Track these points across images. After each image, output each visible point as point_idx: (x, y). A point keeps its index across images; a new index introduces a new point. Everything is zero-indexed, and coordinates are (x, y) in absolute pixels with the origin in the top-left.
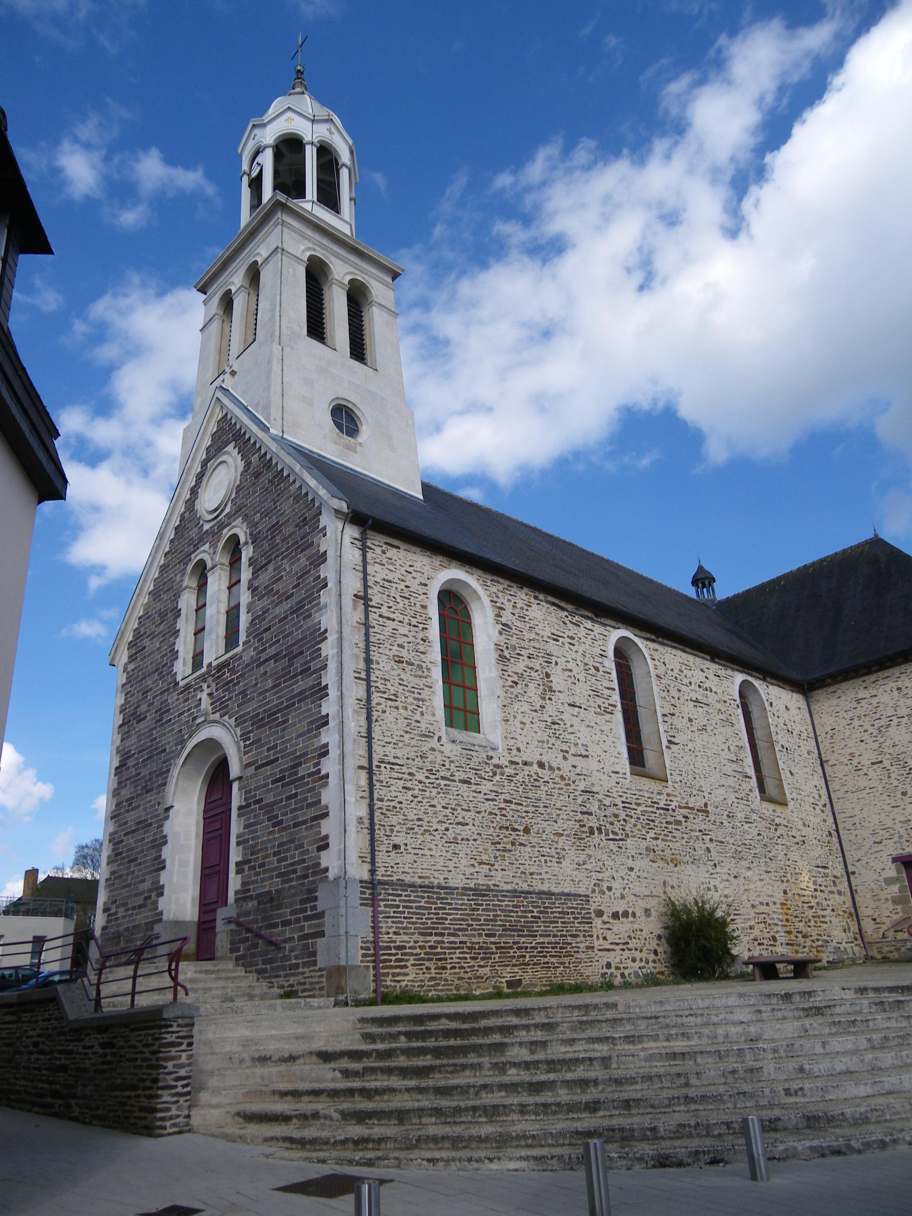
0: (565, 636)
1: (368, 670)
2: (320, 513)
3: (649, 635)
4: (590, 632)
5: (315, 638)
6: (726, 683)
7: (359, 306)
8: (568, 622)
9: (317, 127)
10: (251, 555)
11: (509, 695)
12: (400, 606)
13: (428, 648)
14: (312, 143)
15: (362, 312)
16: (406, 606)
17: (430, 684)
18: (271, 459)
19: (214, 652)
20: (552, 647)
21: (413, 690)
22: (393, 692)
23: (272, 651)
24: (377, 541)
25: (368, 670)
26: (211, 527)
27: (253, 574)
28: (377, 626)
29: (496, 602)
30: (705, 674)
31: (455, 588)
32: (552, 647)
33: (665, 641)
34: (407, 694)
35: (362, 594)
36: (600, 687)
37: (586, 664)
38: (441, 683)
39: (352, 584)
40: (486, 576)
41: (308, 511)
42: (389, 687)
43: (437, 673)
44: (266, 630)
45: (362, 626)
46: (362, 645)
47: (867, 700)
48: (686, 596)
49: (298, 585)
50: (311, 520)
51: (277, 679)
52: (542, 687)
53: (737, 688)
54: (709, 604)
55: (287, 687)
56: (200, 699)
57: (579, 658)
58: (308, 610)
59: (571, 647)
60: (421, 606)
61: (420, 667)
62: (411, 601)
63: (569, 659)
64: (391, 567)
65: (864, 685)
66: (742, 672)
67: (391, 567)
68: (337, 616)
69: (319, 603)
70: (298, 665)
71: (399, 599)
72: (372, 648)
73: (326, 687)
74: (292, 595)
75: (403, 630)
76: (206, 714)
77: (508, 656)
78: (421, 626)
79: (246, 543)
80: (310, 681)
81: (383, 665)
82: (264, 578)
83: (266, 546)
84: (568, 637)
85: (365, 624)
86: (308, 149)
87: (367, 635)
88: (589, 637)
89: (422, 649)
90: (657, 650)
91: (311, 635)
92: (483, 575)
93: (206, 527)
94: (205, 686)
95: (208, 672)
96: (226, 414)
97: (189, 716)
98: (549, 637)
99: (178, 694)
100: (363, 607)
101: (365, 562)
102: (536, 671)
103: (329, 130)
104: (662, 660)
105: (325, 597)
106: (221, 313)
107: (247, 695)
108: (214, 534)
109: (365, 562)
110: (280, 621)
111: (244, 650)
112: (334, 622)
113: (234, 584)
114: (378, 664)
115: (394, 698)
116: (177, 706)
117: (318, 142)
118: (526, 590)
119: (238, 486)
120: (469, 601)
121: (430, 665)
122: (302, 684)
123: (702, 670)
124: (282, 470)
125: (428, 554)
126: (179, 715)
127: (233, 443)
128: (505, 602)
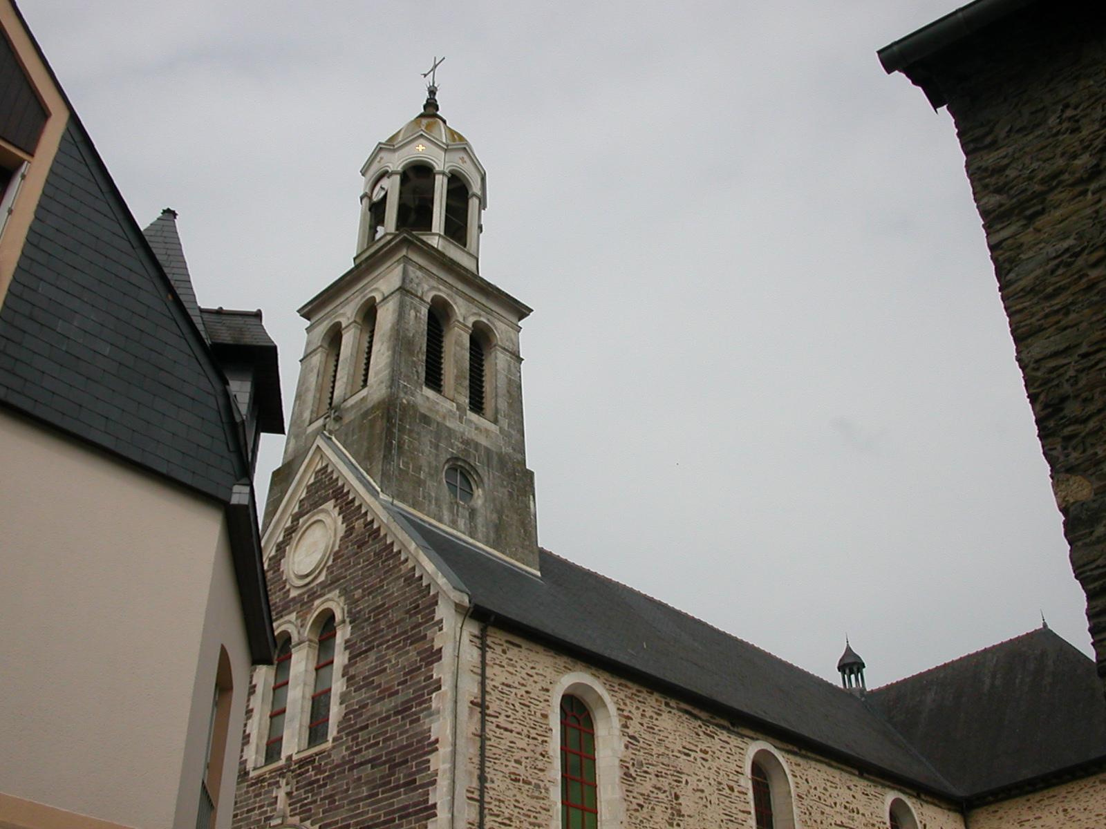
0: (698, 750)
1: (482, 790)
2: (436, 603)
3: (790, 747)
4: (726, 745)
5: (423, 747)
6: (875, 803)
7: (481, 350)
8: (701, 733)
9: (450, 156)
10: (348, 636)
11: (634, 821)
12: (519, 715)
13: (547, 765)
14: (443, 174)
15: (482, 355)
16: (526, 715)
17: (547, 807)
18: (379, 528)
19: (293, 744)
20: (682, 762)
21: (529, 813)
22: (507, 815)
23: (370, 754)
24: (496, 638)
25: (482, 790)
26: (300, 595)
27: (350, 659)
28: (493, 739)
29: (623, 710)
30: (852, 793)
31: (578, 693)
32: (682, 762)
33: (809, 754)
34: (523, 818)
35: (479, 700)
36: (734, 811)
37: (720, 783)
38: (559, 805)
39: (470, 688)
40: (614, 680)
41: (422, 597)
42: (503, 809)
43: (556, 795)
44: (362, 729)
45: (478, 738)
46: (476, 760)
47: (1031, 823)
48: (831, 685)
49: (406, 681)
50: (425, 609)
51: (374, 788)
52: (669, 811)
53: (887, 809)
54: (858, 695)
55: (386, 799)
56: (276, 797)
57: (712, 776)
58: (415, 713)
59: (704, 762)
60: (542, 715)
61: (538, 786)
62: (532, 709)
63: (701, 777)
64: (511, 669)
65: (1029, 804)
66: (893, 788)
67: (511, 669)
68: (447, 723)
69: (429, 708)
70: (400, 776)
71: (518, 707)
72: (487, 764)
73: (434, 806)
74: (397, 692)
75: (521, 743)
76: (284, 817)
77: (634, 775)
78: (540, 739)
79: (343, 622)
80: (416, 796)
81: (499, 784)
82: (364, 666)
83: (367, 629)
84: (701, 750)
85: (480, 736)
86: (439, 178)
87: (482, 748)
88: (724, 751)
89: (540, 765)
90: (799, 765)
91: (418, 742)
92: (610, 679)
93: (293, 594)
94: (283, 782)
95: (288, 766)
96: (327, 466)
97: (261, 814)
98: (679, 752)
99: (249, 786)
100: (480, 715)
101: (484, 664)
102: (665, 792)
103: (462, 159)
104: (804, 777)
105: (436, 701)
106: (326, 346)
107: (335, 801)
108: (304, 603)
109: (484, 664)
110: (381, 720)
111: (334, 747)
112: (448, 732)
113: (323, 664)
114: (493, 782)
115: (508, 822)
116: (246, 800)
117: (450, 172)
118: (656, 695)
119: (337, 553)
120: (593, 708)
121: (548, 785)
122: (403, 799)
123: (849, 788)
124: (392, 544)
125: (552, 653)
126: (248, 811)
127: (333, 501)
128: (633, 710)
